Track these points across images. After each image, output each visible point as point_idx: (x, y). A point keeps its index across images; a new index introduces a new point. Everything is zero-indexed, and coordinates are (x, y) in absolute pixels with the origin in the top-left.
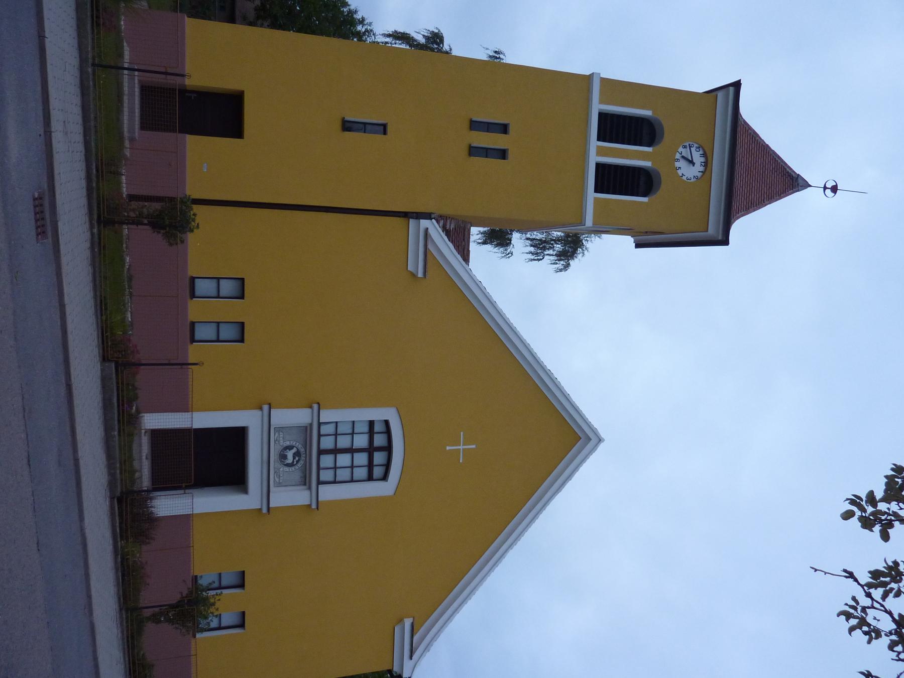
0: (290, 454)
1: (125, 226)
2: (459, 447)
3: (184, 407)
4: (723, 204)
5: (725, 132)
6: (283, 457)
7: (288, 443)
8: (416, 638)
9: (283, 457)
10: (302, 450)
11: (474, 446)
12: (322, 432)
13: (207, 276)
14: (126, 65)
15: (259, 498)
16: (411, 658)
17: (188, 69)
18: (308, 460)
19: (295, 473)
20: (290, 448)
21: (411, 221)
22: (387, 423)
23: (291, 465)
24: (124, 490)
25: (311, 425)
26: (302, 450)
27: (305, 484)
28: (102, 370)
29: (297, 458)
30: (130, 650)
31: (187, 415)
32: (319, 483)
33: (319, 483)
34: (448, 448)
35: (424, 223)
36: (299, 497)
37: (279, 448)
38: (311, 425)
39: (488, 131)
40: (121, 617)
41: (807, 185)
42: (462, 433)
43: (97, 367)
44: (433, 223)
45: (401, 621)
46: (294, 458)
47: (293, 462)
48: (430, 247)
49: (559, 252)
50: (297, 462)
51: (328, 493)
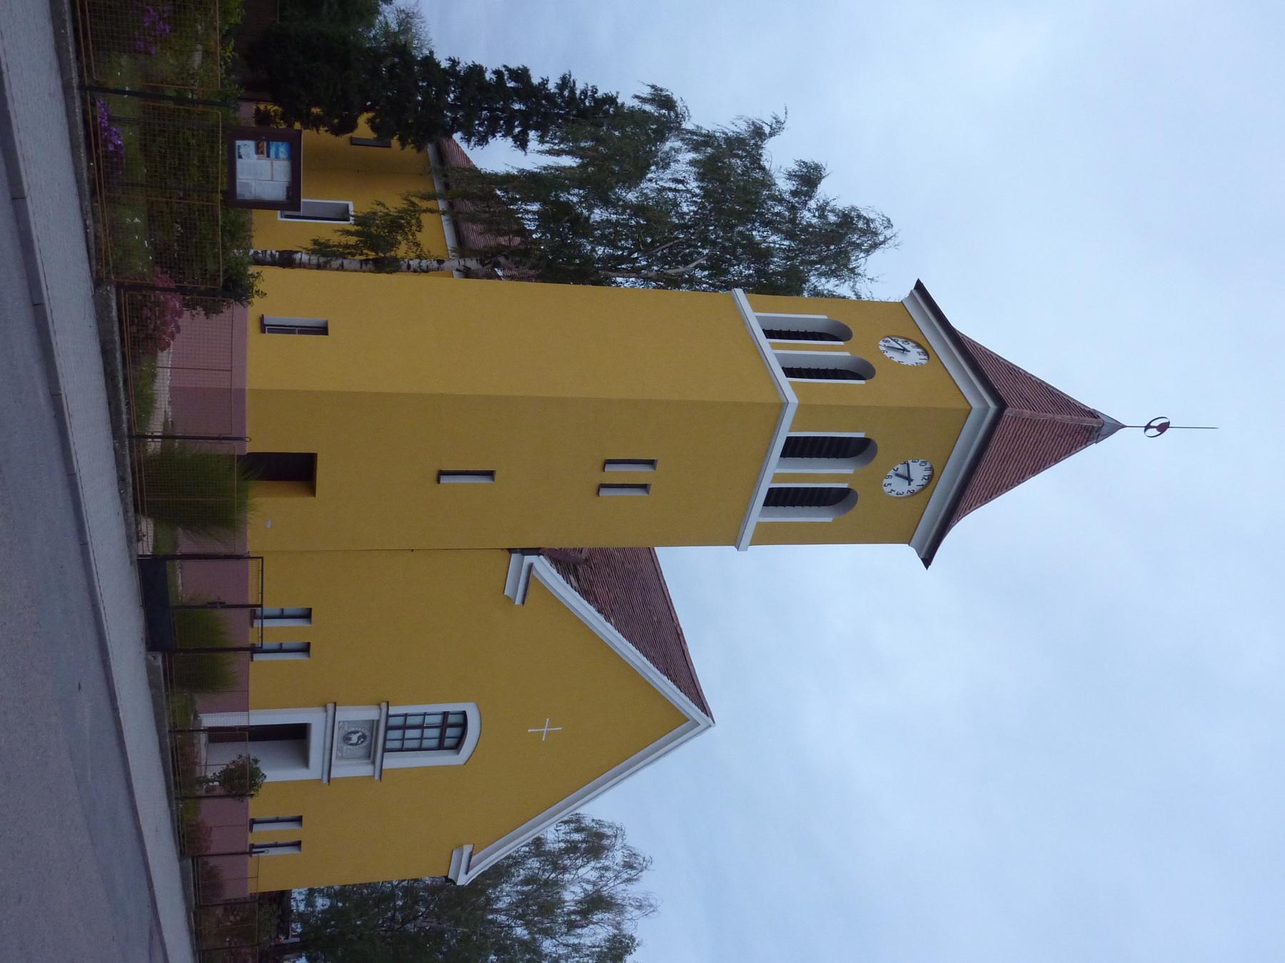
0: (354, 738)
3: (244, 708)
4: (946, 505)
5: (969, 446)
7: (353, 729)
8: (474, 858)
9: (346, 739)
10: (368, 734)
11: (561, 728)
12: (390, 713)
14: (169, 370)
17: (248, 432)
18: (373, 747)
19: (360, 750)
20: (356, 732)
22: (464, 714)
23: (356, 744)
25: (378, 721)
26: (368, 734)
27: (369, 757)
28: (180, 866)
29: (362, 740)
32: (385, 750)
33: (385, 750)
34: (529, 731)
35: (529, 559)
36: (364, 770)
37: (343, 733)
38: (378, 721)
41: (1117, 426)
43: (176, 866)
44: (540, 560)
45: (460, 847)
49: (580, 902)
50: (362, 742)
51: (393, 762)
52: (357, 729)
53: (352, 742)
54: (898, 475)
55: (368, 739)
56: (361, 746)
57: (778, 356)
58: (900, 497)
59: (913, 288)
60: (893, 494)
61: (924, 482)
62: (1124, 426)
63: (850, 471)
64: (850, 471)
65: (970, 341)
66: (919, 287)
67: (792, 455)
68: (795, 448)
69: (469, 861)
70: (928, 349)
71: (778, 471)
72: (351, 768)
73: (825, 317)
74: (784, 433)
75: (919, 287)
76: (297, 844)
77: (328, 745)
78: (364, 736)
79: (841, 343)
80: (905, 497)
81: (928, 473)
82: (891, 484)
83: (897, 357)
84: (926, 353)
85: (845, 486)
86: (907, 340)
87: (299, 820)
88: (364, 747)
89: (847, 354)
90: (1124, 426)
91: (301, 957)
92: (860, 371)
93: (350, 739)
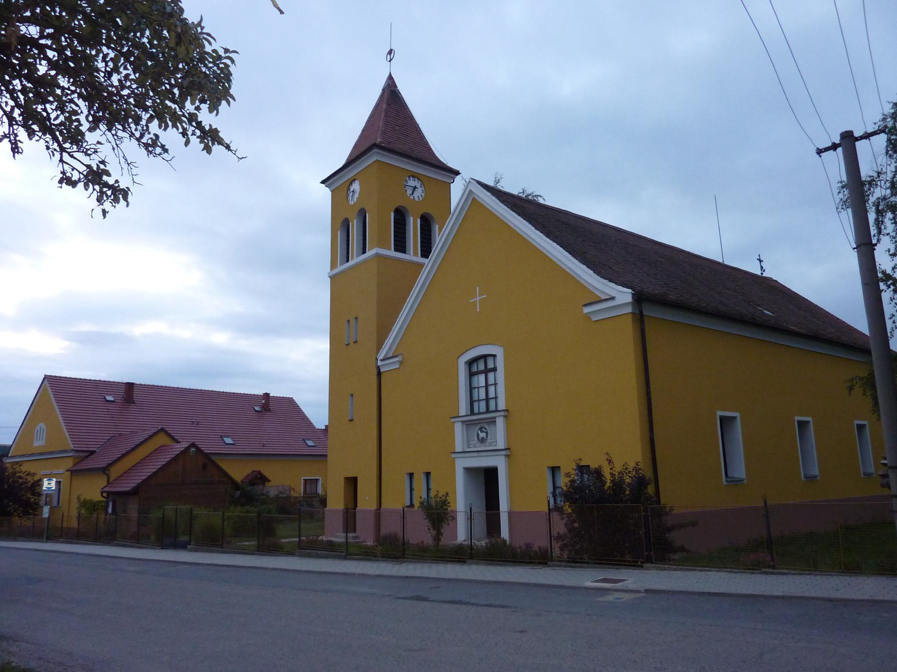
0: (482, 435)
1: (256, 543)
2: (479, 298)
6: (482, 441)
7: (476, 437)
9: (482, 441)
10: (479, 426)
11: (478, 288)
13: (61, 496)
15: (496, 457)
16: (613, 298)
20: (478, 435)
21: (381, 371)
23: (487, 433)
24: (283, 540)
25: (463, 422)
26: (479, 426)
28: (297, 556)
29: (483, 429)
30: (782, 571)
31: (458, 514)
38: (463, 422)
39: (130, 386)
40: (555, 566)
41: (390, 78)
42: (471, 301)
45: (587, 317)
46: (483, 432)
47: (485, 432)
48: (390, 355)
50: (485, 429)
52: (475, 435)
53: (485, 436)
54: (412, 194)
55: (482, 425)
56: (488, 429)
57: (357, 256)
58: (425, 191)
59: (324, 185)
60: (423, 195)
61: (416, 180)
62: (390, 73)
63: (412, 218)
64: (412, 218)
65: (350, 156)
66: (323, 182)
67: (405, 247)
68: (401, 246)
69: (606, 300)
70: (352, 179)
71: (412, 254)
72: (499, 434)
73: (339, 232)
74: (392, 253)
75: (323, 182)
76: (428, 474)
77: (476, 454)
78: (481, 429)
79: (350, 223)
80: (425, 188)
81: (411, 178)
82: (418, 196)
83: (357, 195)
84: (354, 180)
85: (419, 220)
86: (349, 189)
87: (411, 475)
88: (489, 427)
89: (355, 221)
90: (390, 73)
91: (241, 481)
92: (362, 214)
93: (483, 438)
